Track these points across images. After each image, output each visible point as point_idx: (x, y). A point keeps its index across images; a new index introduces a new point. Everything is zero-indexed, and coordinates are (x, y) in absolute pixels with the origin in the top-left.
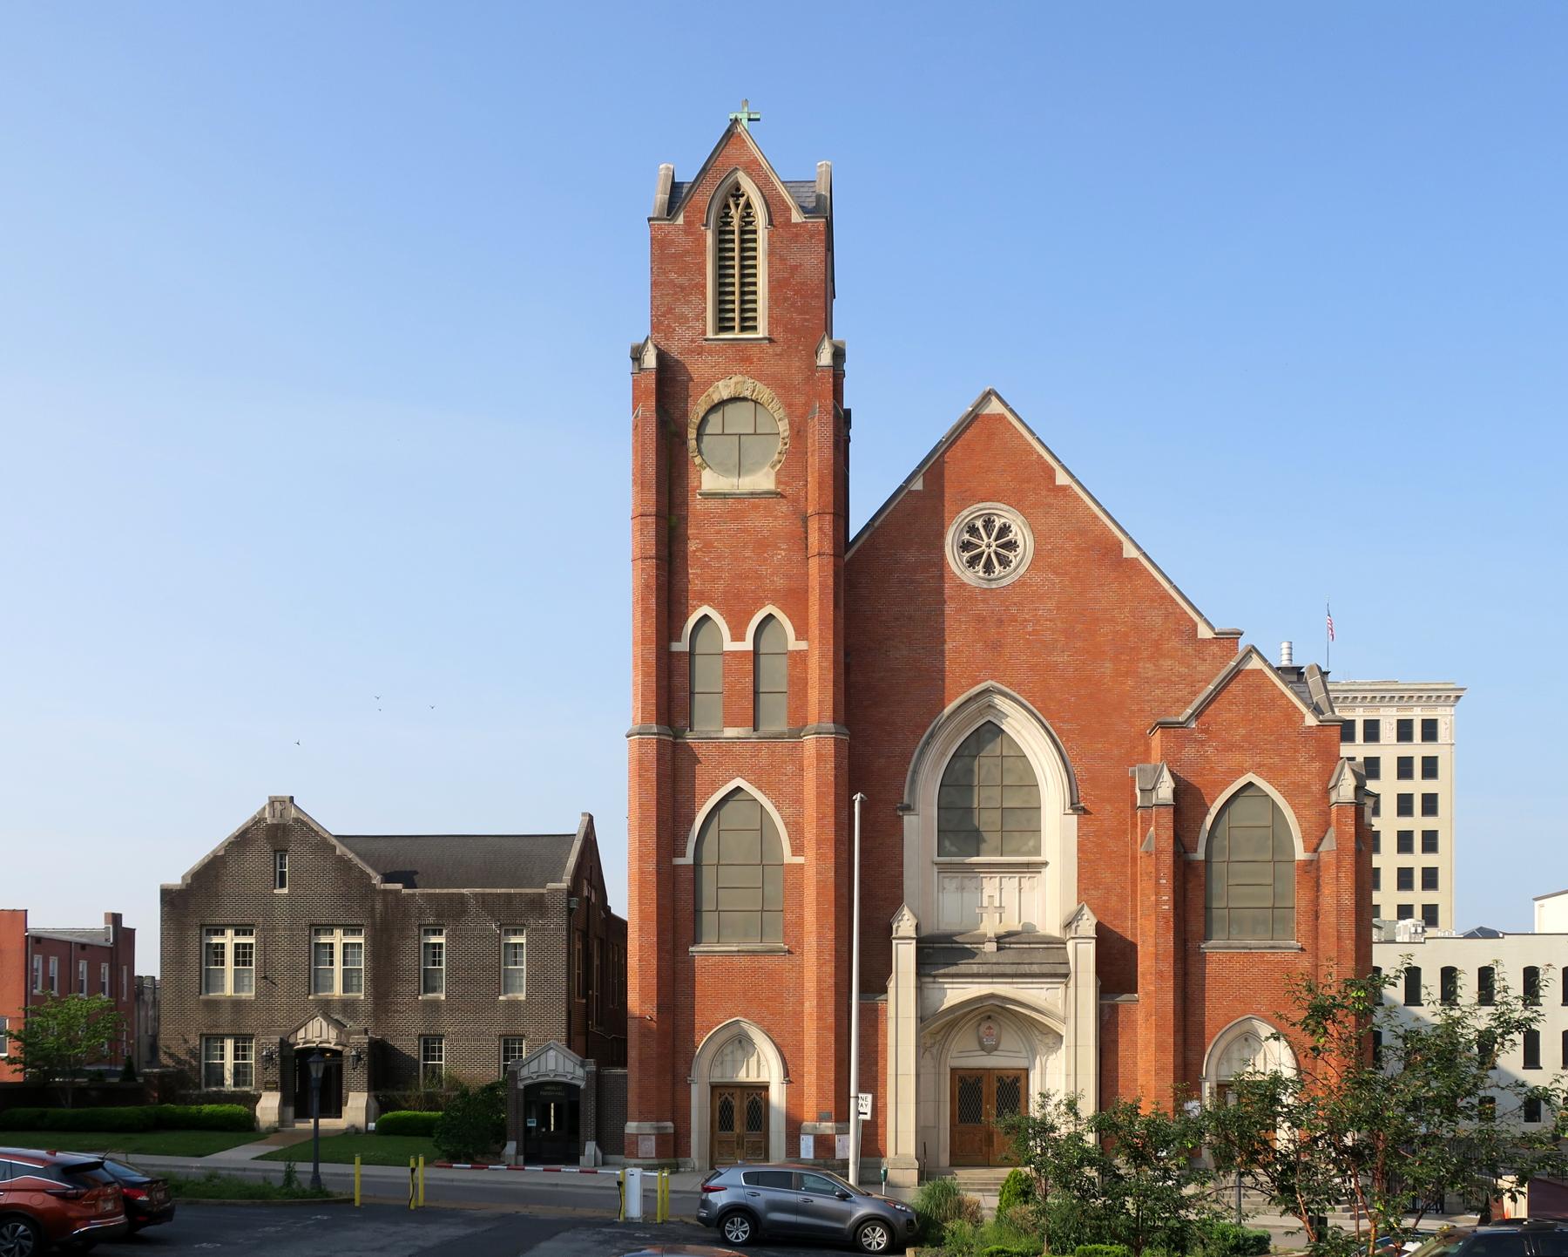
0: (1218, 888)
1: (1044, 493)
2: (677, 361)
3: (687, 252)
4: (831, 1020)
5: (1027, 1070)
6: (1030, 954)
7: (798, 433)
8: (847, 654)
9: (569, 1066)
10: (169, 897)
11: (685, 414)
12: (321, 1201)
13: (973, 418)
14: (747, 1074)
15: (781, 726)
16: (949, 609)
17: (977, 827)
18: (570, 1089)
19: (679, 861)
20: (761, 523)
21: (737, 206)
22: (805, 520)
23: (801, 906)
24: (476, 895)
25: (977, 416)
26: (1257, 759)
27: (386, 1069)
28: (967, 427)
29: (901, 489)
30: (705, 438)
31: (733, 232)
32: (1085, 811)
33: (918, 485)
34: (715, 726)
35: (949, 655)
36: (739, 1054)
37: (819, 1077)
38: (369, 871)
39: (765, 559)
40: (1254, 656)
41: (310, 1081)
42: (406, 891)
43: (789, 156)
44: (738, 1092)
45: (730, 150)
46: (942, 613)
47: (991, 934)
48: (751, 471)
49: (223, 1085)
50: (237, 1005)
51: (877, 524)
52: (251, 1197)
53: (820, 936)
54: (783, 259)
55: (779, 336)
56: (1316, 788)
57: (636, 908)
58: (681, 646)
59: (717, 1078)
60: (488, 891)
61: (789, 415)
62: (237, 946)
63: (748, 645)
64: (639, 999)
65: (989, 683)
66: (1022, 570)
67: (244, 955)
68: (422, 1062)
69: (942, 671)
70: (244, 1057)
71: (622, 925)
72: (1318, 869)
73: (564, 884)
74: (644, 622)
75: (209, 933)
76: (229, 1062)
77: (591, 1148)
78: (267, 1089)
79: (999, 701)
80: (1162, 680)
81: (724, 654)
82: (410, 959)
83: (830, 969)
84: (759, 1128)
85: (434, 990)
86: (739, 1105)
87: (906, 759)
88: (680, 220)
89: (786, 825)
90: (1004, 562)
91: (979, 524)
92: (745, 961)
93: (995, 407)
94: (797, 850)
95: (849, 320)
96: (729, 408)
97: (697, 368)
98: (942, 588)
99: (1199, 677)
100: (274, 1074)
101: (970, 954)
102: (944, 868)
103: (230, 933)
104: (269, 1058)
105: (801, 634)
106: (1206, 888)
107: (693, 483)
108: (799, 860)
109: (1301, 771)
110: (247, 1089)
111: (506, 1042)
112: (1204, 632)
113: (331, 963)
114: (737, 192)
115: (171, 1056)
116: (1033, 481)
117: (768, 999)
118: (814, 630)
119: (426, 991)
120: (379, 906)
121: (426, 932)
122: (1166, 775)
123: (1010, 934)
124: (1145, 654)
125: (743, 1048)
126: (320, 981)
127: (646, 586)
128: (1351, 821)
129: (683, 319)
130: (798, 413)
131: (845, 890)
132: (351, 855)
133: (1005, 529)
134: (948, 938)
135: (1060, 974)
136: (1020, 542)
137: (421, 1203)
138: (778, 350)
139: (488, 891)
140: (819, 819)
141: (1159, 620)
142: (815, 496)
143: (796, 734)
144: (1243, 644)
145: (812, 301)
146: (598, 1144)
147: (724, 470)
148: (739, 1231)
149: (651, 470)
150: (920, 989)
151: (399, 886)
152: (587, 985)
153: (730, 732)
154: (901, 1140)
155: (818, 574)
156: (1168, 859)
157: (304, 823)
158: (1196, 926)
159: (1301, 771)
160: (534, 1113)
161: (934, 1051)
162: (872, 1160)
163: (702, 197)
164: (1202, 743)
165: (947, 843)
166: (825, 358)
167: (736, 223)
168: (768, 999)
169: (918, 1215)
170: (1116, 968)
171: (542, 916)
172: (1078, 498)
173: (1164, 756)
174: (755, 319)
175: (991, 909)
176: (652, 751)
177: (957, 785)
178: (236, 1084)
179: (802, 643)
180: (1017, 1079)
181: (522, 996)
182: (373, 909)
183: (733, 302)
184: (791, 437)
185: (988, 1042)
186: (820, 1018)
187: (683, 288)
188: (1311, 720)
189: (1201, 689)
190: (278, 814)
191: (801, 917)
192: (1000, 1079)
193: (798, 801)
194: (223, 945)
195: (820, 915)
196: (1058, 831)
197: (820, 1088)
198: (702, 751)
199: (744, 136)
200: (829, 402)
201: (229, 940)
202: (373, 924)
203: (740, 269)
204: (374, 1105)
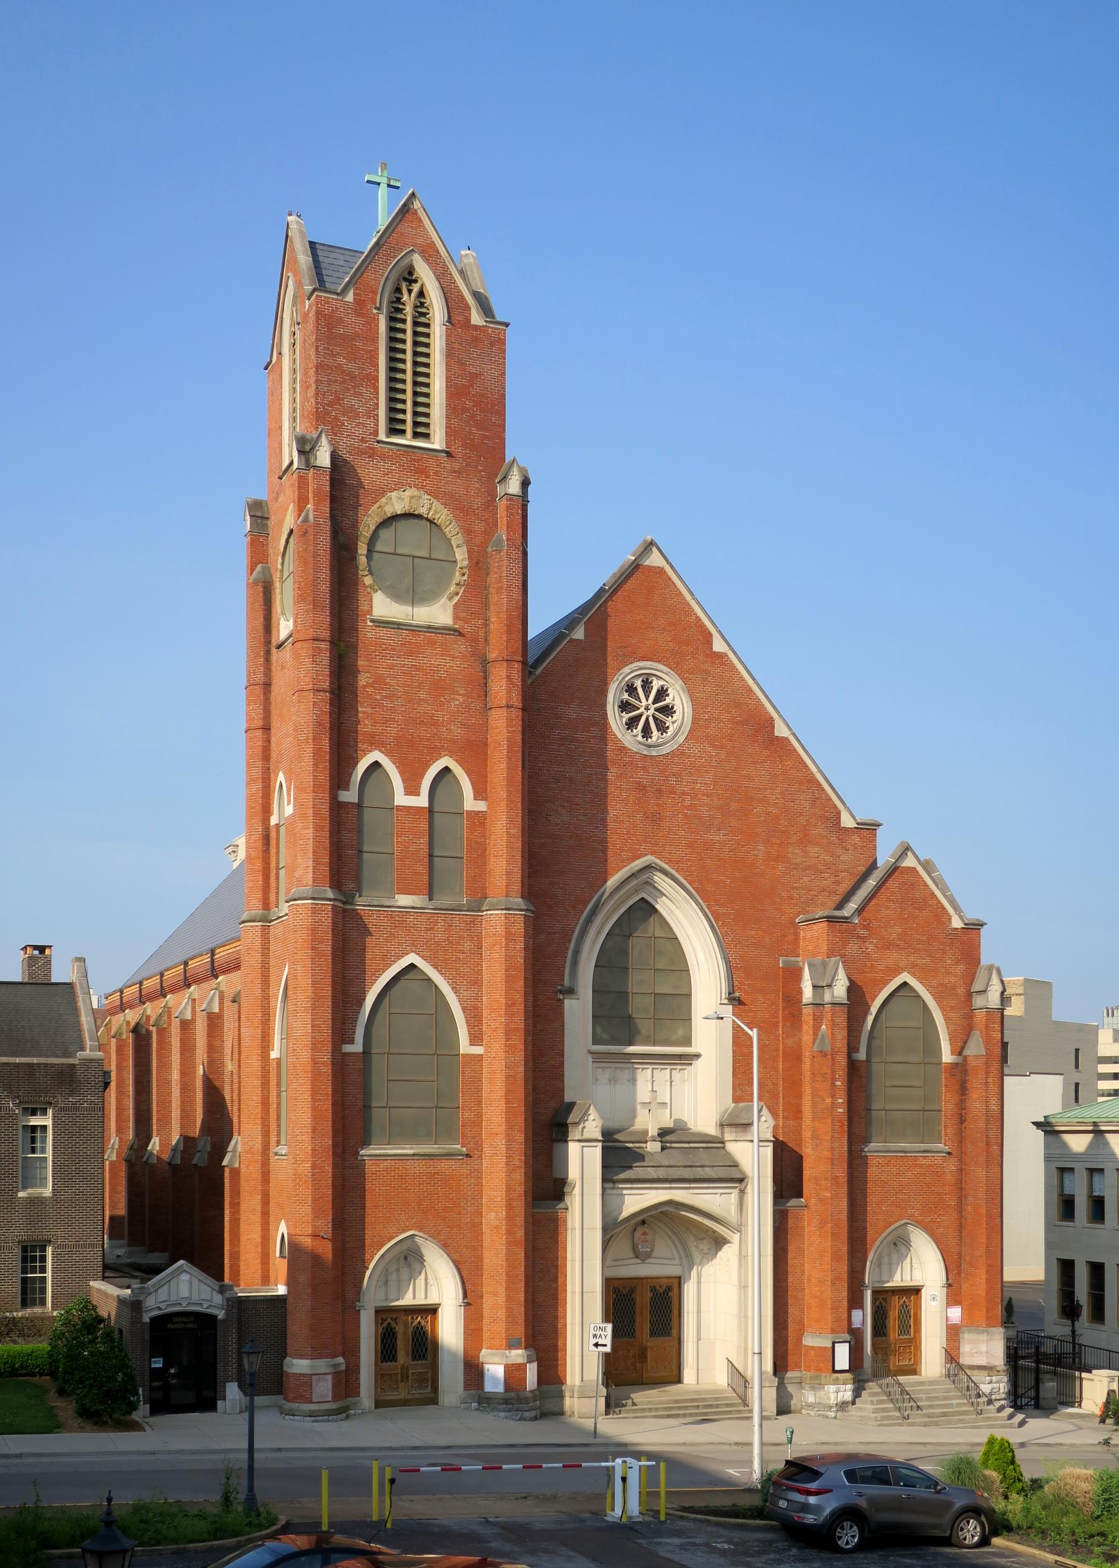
3: (356, 336)
5: (679, 1281)
6: (697, 1156)
11: (355, 525)
13: (634, 568)
17: (637, 1013)
19: (348, 1048)
21: (410, 291)
26: (911, 959)
28: (629, 577)
30: (375, 556)
31: (404, 321)
35: (611, 825)
36: (405, 1272)
39: (442, 704)
45: (405, 227)
46: (604, 779)
54: (461, 364)
55: (457, 450)
56: (961, 991)
58: (350, 796)
61: (468, 542)
63: (422, 801)
65: (649, 859)
66: (681, 739)
69: (604, 841)
77: (232, 1391)
79: (659, 879)
80: (809, 868)
84: (424, 1358)
89: (464, 1009)
90: (662, 728)
91: (638, 683)
92: (419, 1166)
93: (654, 560)
94: (476, 1038)
95: (518, 445)
96: (402, 524)
97: (369, 473)
99: (842, 867)
102: (599, 1058)
105: (480, 793)
107: (364, 607)
108: (478, 1050)
111: (24, 1249)
112: (847, 822)
114: (409, 276)
116: (691, 646)
124: (794, 839)
125: (409, 1266)
127: (319, 724)
130: (477, 541)
133: (662, 693)
136: (678, 708)
138: (457, 466)
140: (508, 1006)
141: (807, 804)
145: (481, 413)
147: (397, 595)
148: (849, 1536)
162: (553, 1387)
164: (863, 939)
168: (445, 1209)
171: (72, 1093)
172: (734, 667)
177: (613, 963)
179: (487, 804)
180: (669, 1288)
181: (47, 1192)
184: (470, 567)
185: (642, 1249)
192: (653, 1289)
193: (477, 983)
198: (371, 922)
203: (397, 367)
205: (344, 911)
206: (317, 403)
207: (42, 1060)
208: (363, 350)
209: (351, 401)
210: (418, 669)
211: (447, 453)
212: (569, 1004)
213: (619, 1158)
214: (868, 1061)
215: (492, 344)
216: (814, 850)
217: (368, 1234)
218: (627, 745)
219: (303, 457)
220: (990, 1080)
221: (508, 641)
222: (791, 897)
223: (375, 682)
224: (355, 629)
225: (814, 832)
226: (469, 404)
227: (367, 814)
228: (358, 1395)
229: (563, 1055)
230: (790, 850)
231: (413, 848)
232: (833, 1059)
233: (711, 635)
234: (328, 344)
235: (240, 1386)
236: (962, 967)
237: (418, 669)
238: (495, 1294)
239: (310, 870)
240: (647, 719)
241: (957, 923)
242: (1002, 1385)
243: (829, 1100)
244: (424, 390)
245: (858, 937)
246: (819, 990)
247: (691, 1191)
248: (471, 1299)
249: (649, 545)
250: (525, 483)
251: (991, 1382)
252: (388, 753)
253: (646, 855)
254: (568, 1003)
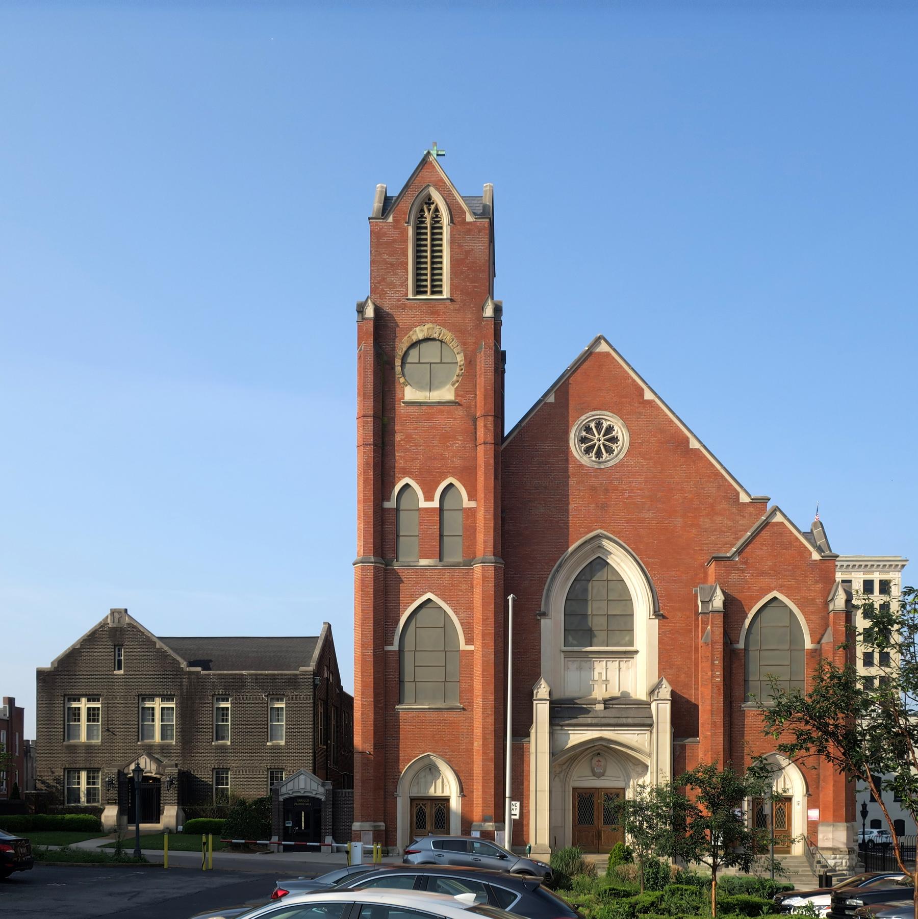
0: (753, 667)
1: (636, 405)
2: (388, 313)
3: (394, 241)
4: (492, 754)
5: (624, 790)
7: (470, 362)
8: (502, 512)
9: (314, 786)
10: (42, 676)
11: (394, 349)
12: (140, 863)
13: (588, 355)
14: (435, 791)
15: (459, 558)
16: (572, 482)
17: (594, 625)
18: (315, 801)
20: (445, 422)
21: (429, 210)
22: (475, 421)
23: (472, 679)
24: (251, 675)
25: (591, 353)
26: (780, 582)
27: (190, 790)
32: (664, 617)
33: (551, 399)
34: (414, 559)
36: (429, 777)
37: (484, 792)
38: (179, 659)
39: (448, 447)
40: (778, 513)
41: (139, 798)
42: (204, 672)
43: (466, 178)
44: (429, 803)
45: (424, 173)
47: (600, 698)
48: (438, 387)
49: (79, 802)
50: (89, 748)
51: (523, 425)
52: (92, 861)
53: (484, 698)
54: (460, 246)
55: (457, 297)
56: (819, 601)
57: (359, 680)
58: (391, 504)
59: (415, 793)
60: (259, 672)
61: (464, 351)
62: (89, 709)
63: (436, 504)
64: (362, 738)
65: (599, 531)
66: (621, 456)
67: (94, 715)
68: (215, 787)
69: (567, 523)
70: (94, 783)
71: (350, 699)
72: (820, 655)
73: (311, 667)
74: (365, 487)
75: (70, 700)
76: (83, 786)
78: (109, 804)
79: (607, 544)
81: (420, 510)
82: (206, 719)
83: (491, 720)
85: (223, 738)
86: (429, 811)
87: (543, 581)
88: (390, 219)
89: (462, 624)
90: (609, 451)
91: (593, 425)
92: (434, 715)
93: (603, 347)
94: (469, 641)
96: (424, 346)
97: (401, 318)
98: (567, 468)
100: (114, 794)
101: (586, 711)
102: (568, 655)
103: (84, 700)
104: (110, 783)
105: (472, 497)
106: (745, 667)
108: (471, 648)
109: (809, 590)
110: (95, 804)
111: (272, 773)
112: (744, 498)
113: (153, 721)
114: (429, 201)
115: (43, 782)
116: (629, 397)
118: (481, 494)
119: (217, 739)
120: (185, 682)
121: (218, 700)
122: (719, 592)
123: (612, 699)
124: (704, 512)
125: (432, 774)
126: (145, 733)
127: (366, 464)
128: (843, 623)
129: (392, 286)
131: (501, 667)
132: (166, 648)
133: (610, 429)
134: (571, 701)
135: (647, 724)
136: (620, 437)
137: (210, 867)
138: (457, 307)
139: (259, 672)
140: (484, 620)
142: (481, 404)
143: (469, 563)
144: (770, 506)
145: (479, 274)
146: (333, 838)
147: (420, 387)
149: (370, 387)
150: (552, 734)
151: (199, 669)
152: (327, 737)
153: (424, 562)
154: (540, 834)
155: (484, 456)
156: (719, 647)
157: (134, 627)
158: (738, 692)
159: (809, 590)
160: (290, 817)
161: (561, 776)
163: (405, 204)
164: (743, 571)
165: (570, 638)
166: (489, 312)
169: (553, 870)
170: (684, 721)
171: (295, 689)
172: (659, 408)
173: (717, 579)
174: (441, 286)
175: (600, 682)
176: (370, 574)
178: (88, 801)
179: (473, 502)
181: (283, 743)
182: (181, 685)
183: (426, 275)
186: (484, 753)
187: (392, 265)
188: (816, 556)
189: (742, 536)
190: (116, 621)
191: (472, 686)
193: (470, 608)
194: (79, 709)
195: (485, 684)
196: (645, 629)
197: (484, 799)
198: (403, 576)
199: (435, 163)
200: (491, 341)
201: (83, 705)
202: (182, 694)
203: (430, 255)
204: (182, 814)
207: (280, 672)
209: (391, 278)
212: (544, 623)
213: (565, 711)
214: (746, 649)
216: (719, 519)
217: (401, 754)
218: (584, 463)
220: (837, 658)
221: (485, 404)
222: (702, 550)
224: (393, 409)
226: (465, 269)
227: (402, 515)
229: (540, 653)
231: (430, 532)
232: (712, 647)
233: (643, 390)
236: (820, 586)
237: (432, 427)
238: (478, 790)
242: (844, 861)
243: (710, 673)
244: (439, 266)
245: (738, 569)
246: (706, 604)
248: (464, 792)
249: (598, 340)
250: (498, 310)
251: (835, 858)
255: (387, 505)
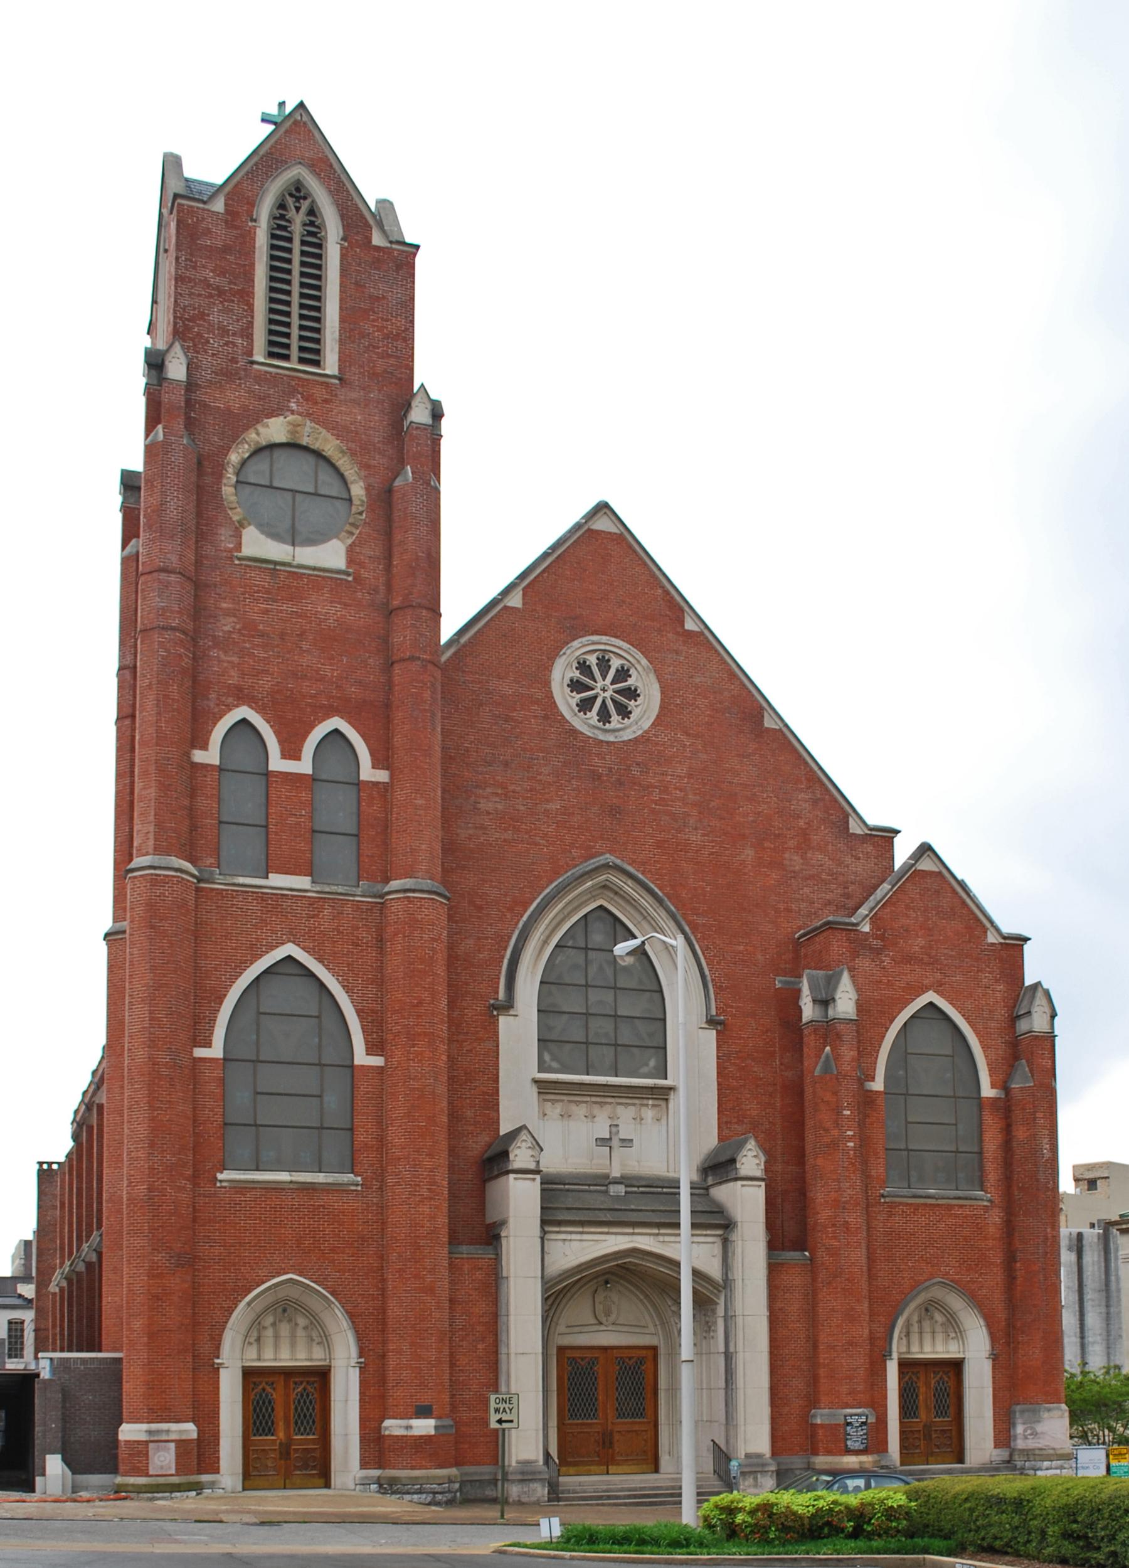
21: (298, 209)
29: (493, 603)
51: (463, 640)
56: (1001, 1013)
65: (609, 858)
77: (54, 1464)
89: (358, 1012)
90: (624, 712)
96: (280, 456)
114: (298, 191)
117: (333, 1250)
124: (791, 843)
164: (878, 952)
167: (297, 229)
168: (333, 1250)
187: (221, 292)
196: (692, 1051)
205: (198, 889)
206: (175, 317)
208: (236, 264)
210: (300, 616)
211: (340, 379)
215: (399, 268)
219: (154, 372)
222: (789, 910)
223: (244, 628)
225: (815, 838)
228: (217, 1471)
230: (787, 855)
234: (191, 255)
235: (64, 1460)
239: (151, 836)
240: (604, 701)
241: (992, 938)
247: (661, 1238)
252: (261, 710)
253: (602, 854)
254: (502, 1020)
255: (199, 756)
